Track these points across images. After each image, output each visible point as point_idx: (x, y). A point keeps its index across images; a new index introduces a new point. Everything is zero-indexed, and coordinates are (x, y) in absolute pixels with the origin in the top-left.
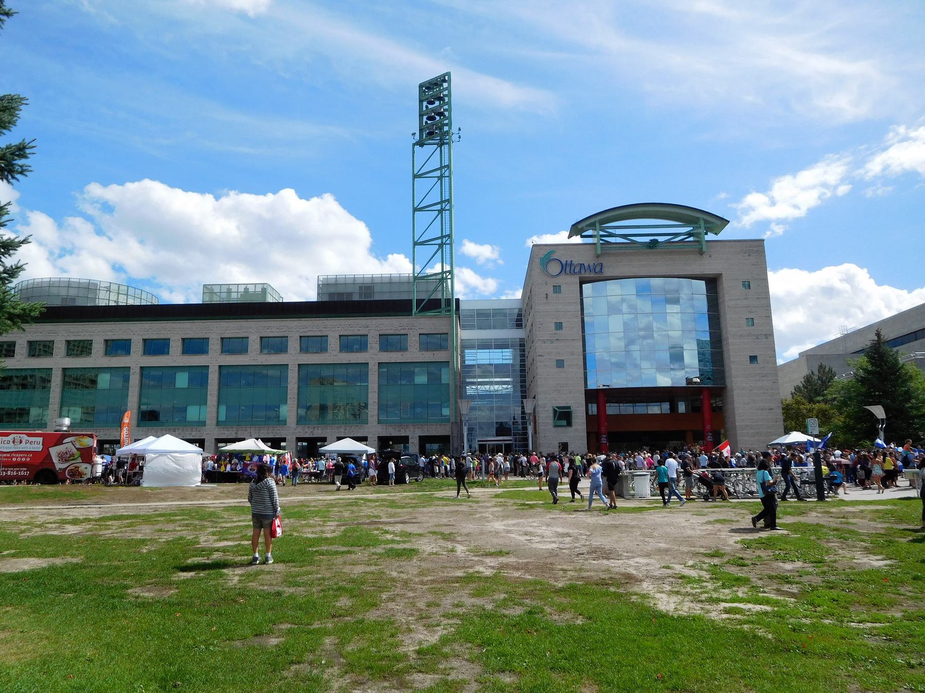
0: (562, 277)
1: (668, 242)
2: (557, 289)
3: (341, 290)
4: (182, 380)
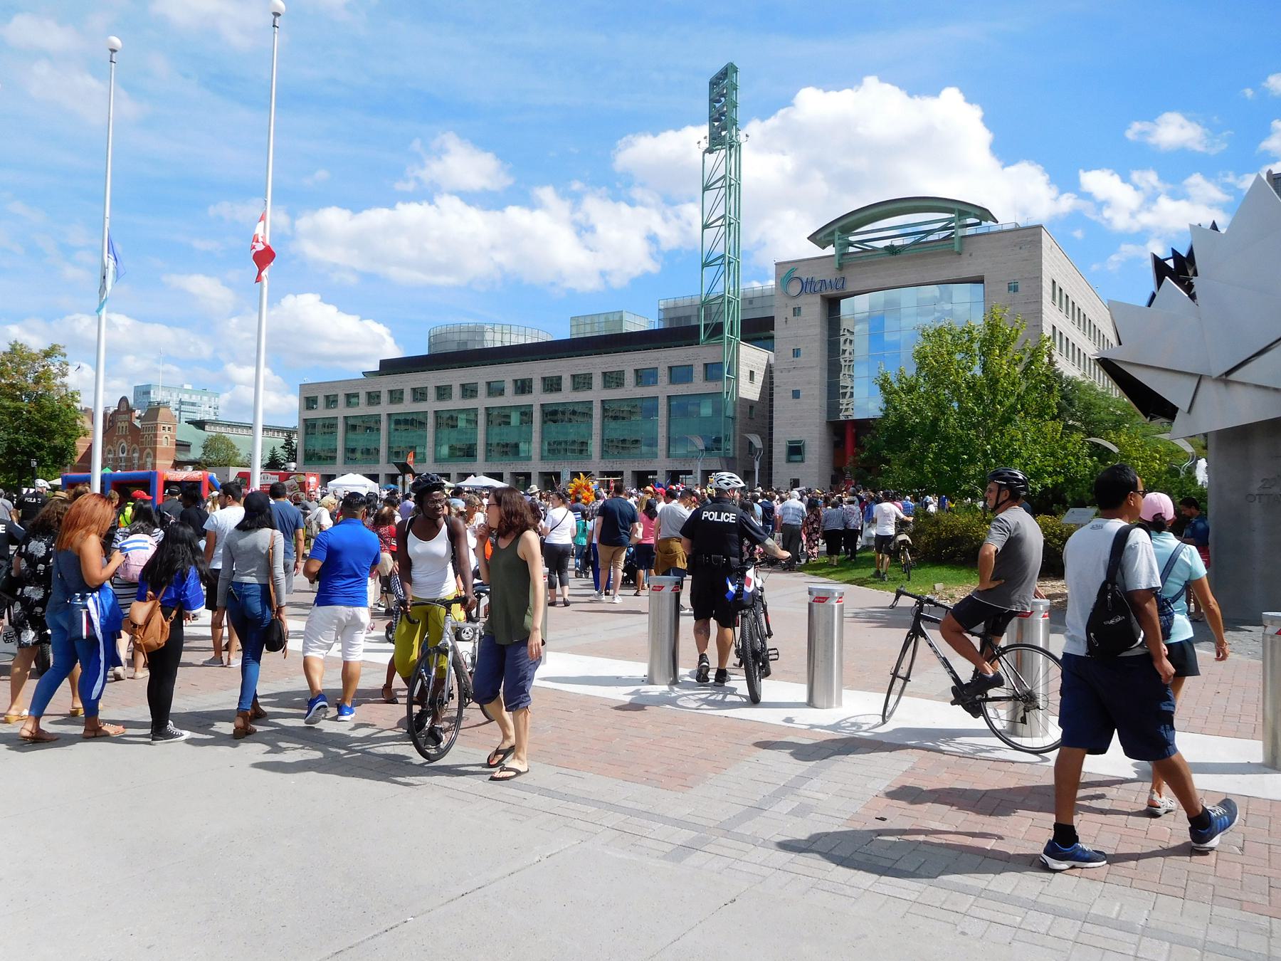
0: (803, 296)
1: (915, 243)
2: (797, 311)
3: (680, 313)
4: (515, 419)
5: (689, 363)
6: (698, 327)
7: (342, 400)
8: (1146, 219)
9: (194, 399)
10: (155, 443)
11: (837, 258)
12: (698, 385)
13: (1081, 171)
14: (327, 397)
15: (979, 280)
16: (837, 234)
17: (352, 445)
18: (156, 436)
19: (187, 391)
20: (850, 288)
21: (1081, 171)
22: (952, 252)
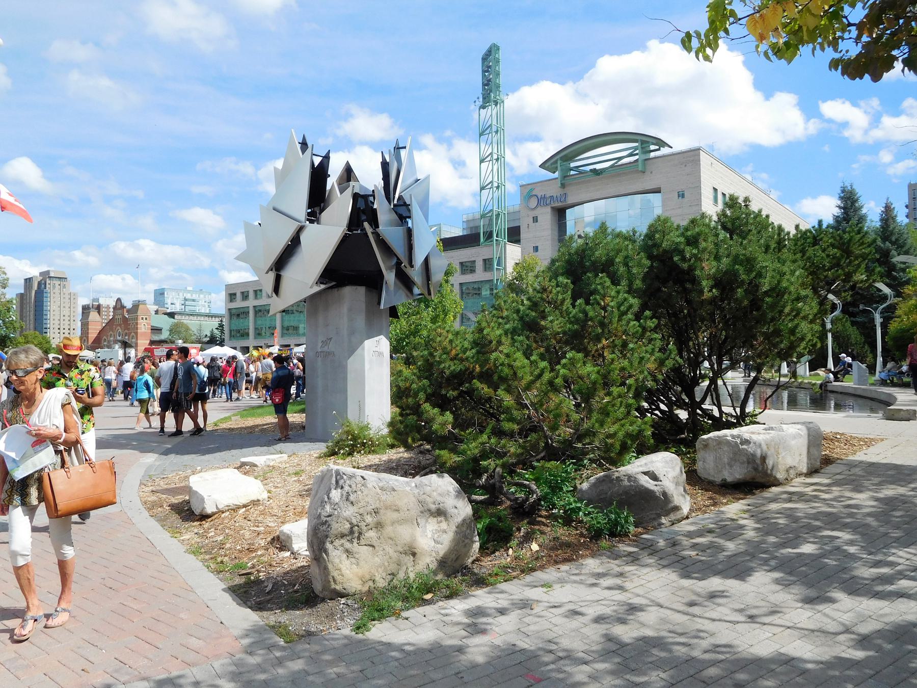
0: (539, 208)
2: (535, 220)
5: (473, 259)
6: (479, 234)
7: (251, 295)
8: (877, 134)
9: (195, 296)
10: (137, 329)
11: (559, 180)
12: (480, 275)
13: (820, 102)
14: (243, 293)
15: (657, 191)
16: (559, 162)
17: (286, 324)
18: (137, 324)
19: (189, 291)
20: (570, 201)
21: (820, 102)
22: (637, 171)
